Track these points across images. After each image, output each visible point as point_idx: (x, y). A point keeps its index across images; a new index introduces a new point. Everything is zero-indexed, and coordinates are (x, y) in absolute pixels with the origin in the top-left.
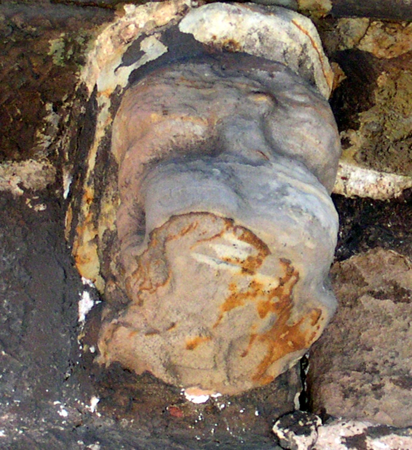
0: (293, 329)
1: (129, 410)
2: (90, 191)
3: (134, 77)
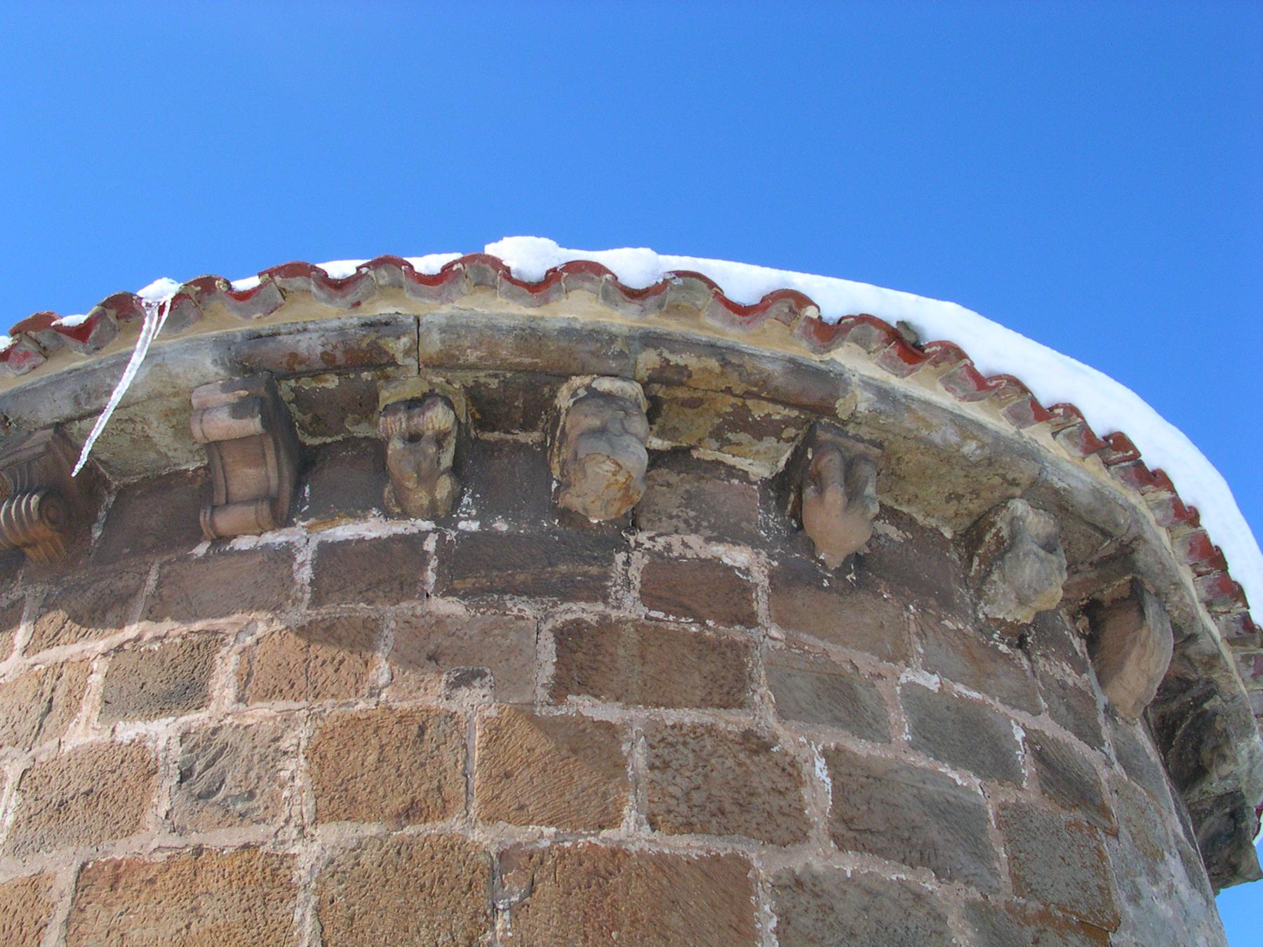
0: (630, 497)
1: (569, 525)
2: (557, 444)
3: (575, 403)
